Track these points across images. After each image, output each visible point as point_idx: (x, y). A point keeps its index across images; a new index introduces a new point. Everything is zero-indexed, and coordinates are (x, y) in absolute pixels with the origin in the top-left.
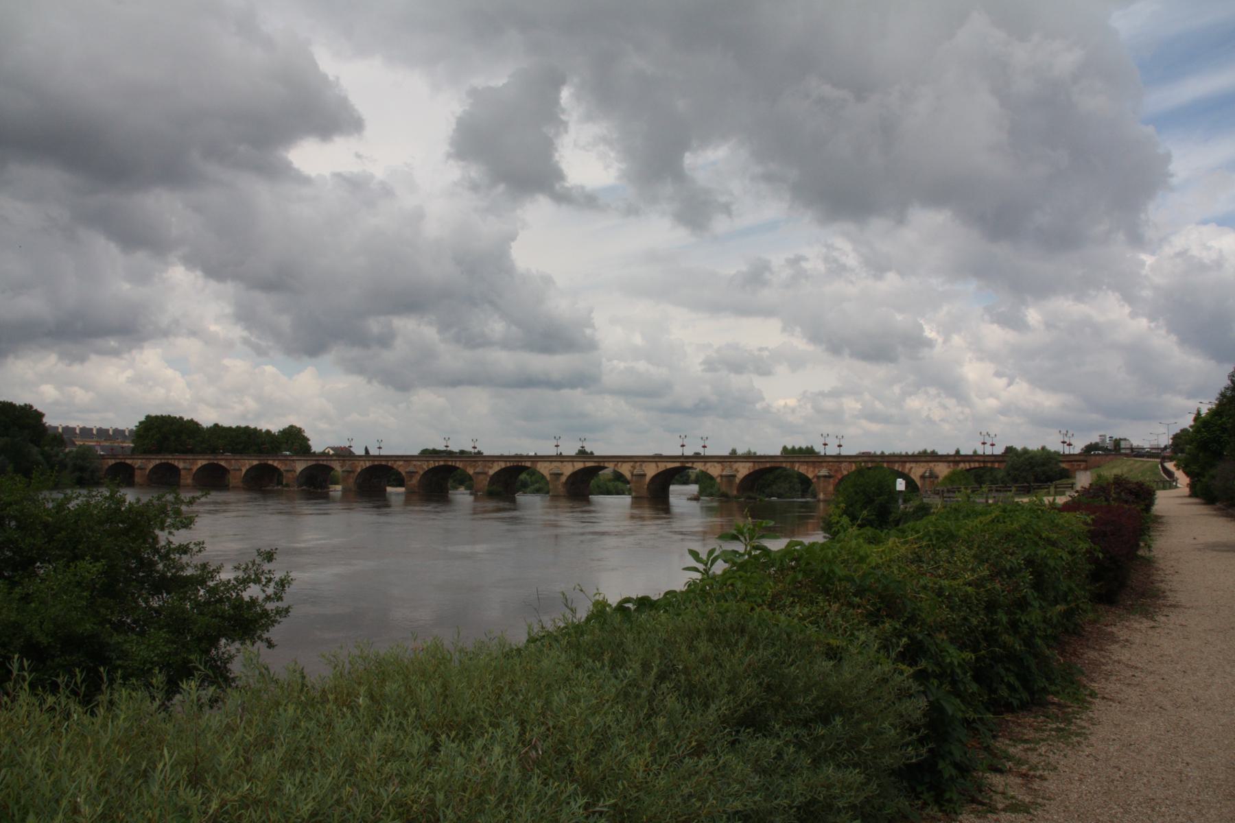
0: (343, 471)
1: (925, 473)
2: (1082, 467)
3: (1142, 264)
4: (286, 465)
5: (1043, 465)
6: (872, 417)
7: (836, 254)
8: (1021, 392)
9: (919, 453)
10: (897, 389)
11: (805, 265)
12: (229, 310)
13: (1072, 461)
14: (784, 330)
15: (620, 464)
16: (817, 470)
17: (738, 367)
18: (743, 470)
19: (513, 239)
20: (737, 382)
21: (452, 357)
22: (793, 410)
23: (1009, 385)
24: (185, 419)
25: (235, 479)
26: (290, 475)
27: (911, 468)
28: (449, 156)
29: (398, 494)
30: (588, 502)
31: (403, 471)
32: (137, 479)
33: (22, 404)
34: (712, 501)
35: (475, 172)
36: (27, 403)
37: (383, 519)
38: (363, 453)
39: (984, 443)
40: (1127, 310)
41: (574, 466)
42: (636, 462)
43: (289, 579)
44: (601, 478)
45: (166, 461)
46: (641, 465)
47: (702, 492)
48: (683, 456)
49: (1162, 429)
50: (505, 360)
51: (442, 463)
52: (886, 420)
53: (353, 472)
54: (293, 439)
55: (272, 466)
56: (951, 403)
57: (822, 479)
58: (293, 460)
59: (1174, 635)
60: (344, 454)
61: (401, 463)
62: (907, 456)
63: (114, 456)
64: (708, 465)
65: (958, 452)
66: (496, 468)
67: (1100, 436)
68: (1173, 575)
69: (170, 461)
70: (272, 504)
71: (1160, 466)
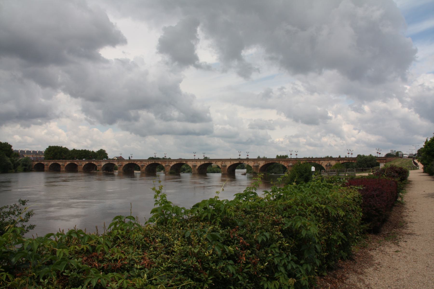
0: (118, 165)
1: (327, 164)
2: (384, 162)
3: (406, 88)
4: (98, 163)
5: (370, 161)
6: (310, 144)
7: (296, 86)
8: (363, 135)
9: (326, 157)
10: (319, 135)
11: (285, 90)
12: (80, 108)
13: (381, 160)
14: (277, 114)
15: (217, 162)
16: (288, 164)
17: (262, 127)
18: (262, 164)
19: (180, 82)
20: (262, 132)
21: (160, 124)
22: (282, 142)
23: (359, 132)
24: (63, 147)
25: (80, 168)
26: (99, 167)
27: (322, 163)
28: (157, 53)
29: (139, 173)
30: (206, 176)
31: (140, 165)
32: (45, 169)
33: (4, 142)
34: (250, 175)
35: (167, 57)
36: (6, 142)
37: (133, 182)
38: (128, 159)
39: (349, 153)
40: (400, 105)
41: (201, 163)
42: (223, 161)
43: (33, 213)
44: (213, 167)
45: (55, 162)
46: (225, 162)
47: (248, 172)
48: (240, 159)
49: (414, 148)
50: (179, 125)
51: (153, 162)
52: (315, 145)
53: (122, 166)
54: (102, 154)
55: (93, 164)
56: (338, 139)
57: (290, 167)
58: (101, 162)
59: (408, 258)
60: (120, 159)
61: (139, 162)
62: (321, 158)
63: (37, 161)
64: (249, 162)
65: (340, 157)
66: (173, 163)
67: (391, 150)
68: (413, 212)
69: (57, 162)
70: (95, 177)
71: (412, 161)
